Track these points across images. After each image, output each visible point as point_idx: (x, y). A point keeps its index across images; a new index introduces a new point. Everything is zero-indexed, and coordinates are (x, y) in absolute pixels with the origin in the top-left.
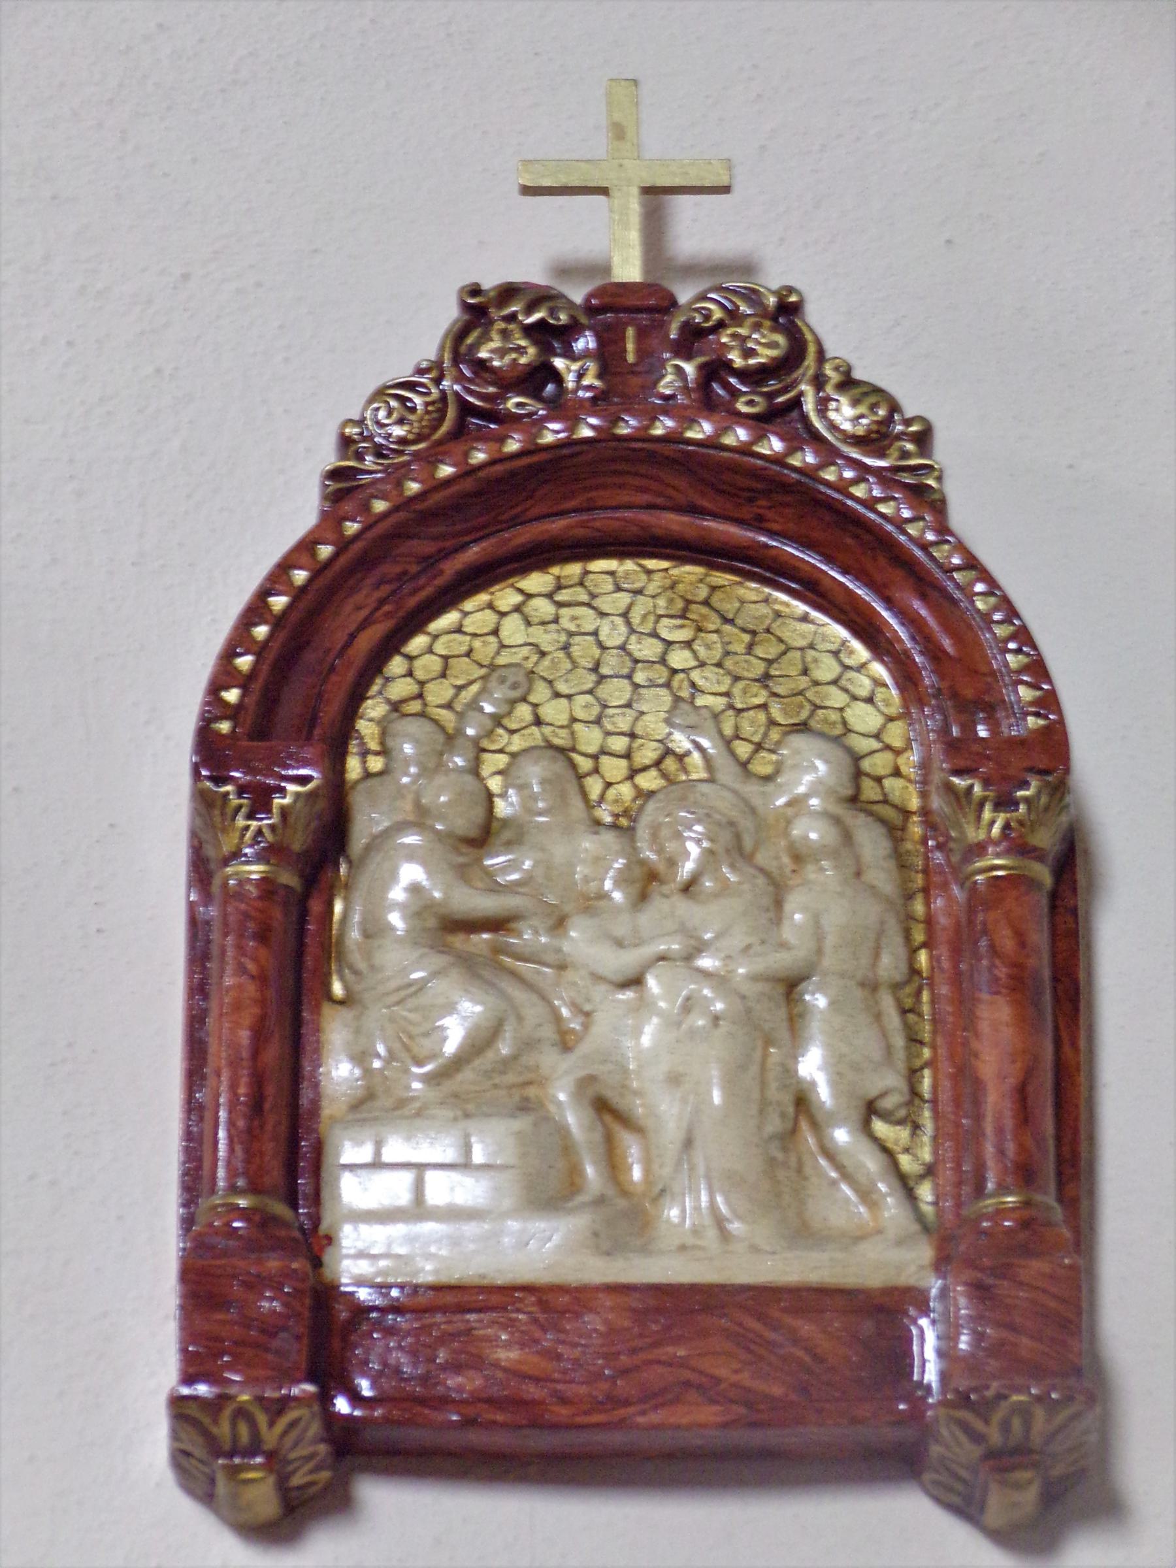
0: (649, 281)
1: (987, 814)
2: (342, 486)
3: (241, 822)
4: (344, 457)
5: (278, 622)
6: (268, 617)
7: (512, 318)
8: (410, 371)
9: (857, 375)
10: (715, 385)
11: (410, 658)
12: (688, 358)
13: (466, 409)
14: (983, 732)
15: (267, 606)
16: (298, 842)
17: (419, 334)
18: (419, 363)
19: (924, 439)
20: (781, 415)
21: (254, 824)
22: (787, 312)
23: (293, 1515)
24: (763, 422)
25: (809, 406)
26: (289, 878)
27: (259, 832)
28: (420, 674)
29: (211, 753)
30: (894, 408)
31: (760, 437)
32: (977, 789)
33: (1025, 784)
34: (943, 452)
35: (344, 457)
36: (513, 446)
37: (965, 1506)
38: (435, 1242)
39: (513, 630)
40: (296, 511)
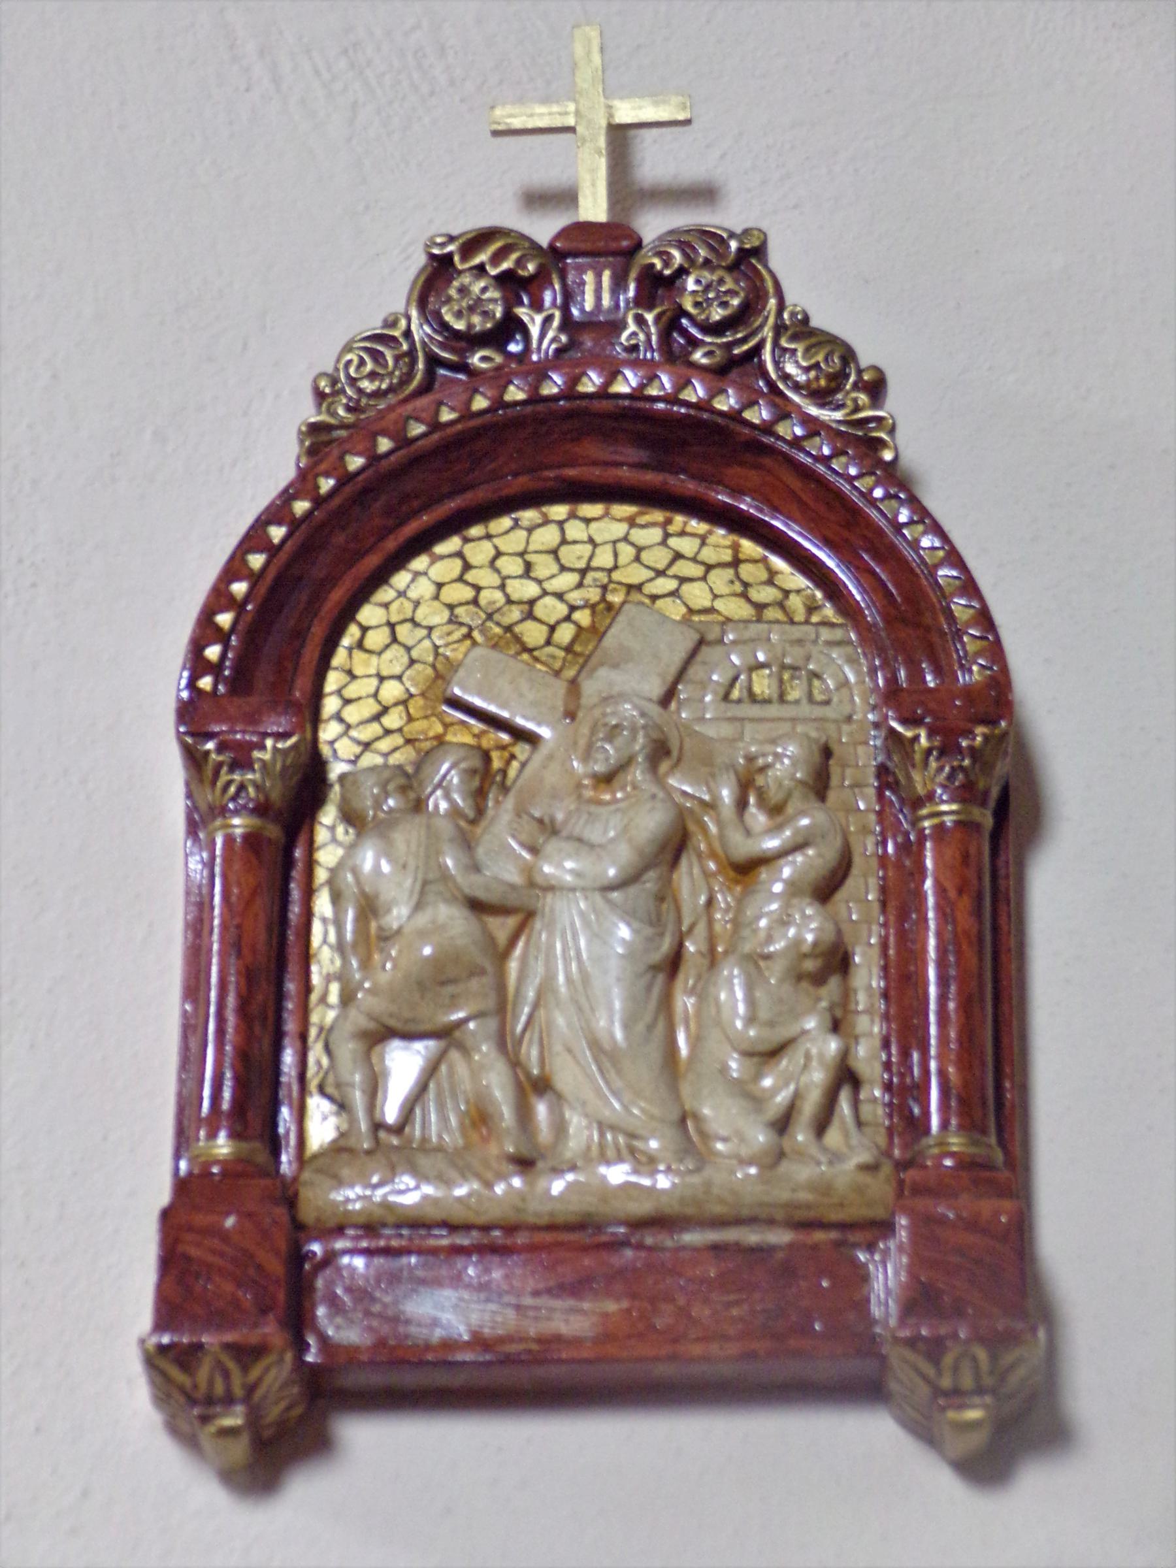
0: (617, 220)
1: (933, 764)
2: (319, 441)
3: (224, 777)
4: (319, 413)
5: (255, 579)
6: (245, 572)
7: (481, 269)
8: (379, 323)
9: (815, 323)
10: (675, 335)
11: (364, 629)
12: (650, 308)
13: (433, 361)
14: (930, 680)
15: (245, 562)
16: (276, 793)
17: (385, 292)
18: (300, 430)
19: (876, 388)
20: (737, 366)
21: (237, 777)
22: (747, 259)
23: (273, 1451)
24: (721, 372)
25: (767, 355)
26: (273, 831)
27: (242, 787)
28: (457, 564)
29: (193, 714)
30: (848, 356)
31: (714, 393)
32: (924, 741)
33: (969, 734)
34: (894, 405)
35: (319, 413)
36: (480, 403)
37: (925, 1431)
38: (356, 1226)
39: (352, 714)
40: (276, 464)
